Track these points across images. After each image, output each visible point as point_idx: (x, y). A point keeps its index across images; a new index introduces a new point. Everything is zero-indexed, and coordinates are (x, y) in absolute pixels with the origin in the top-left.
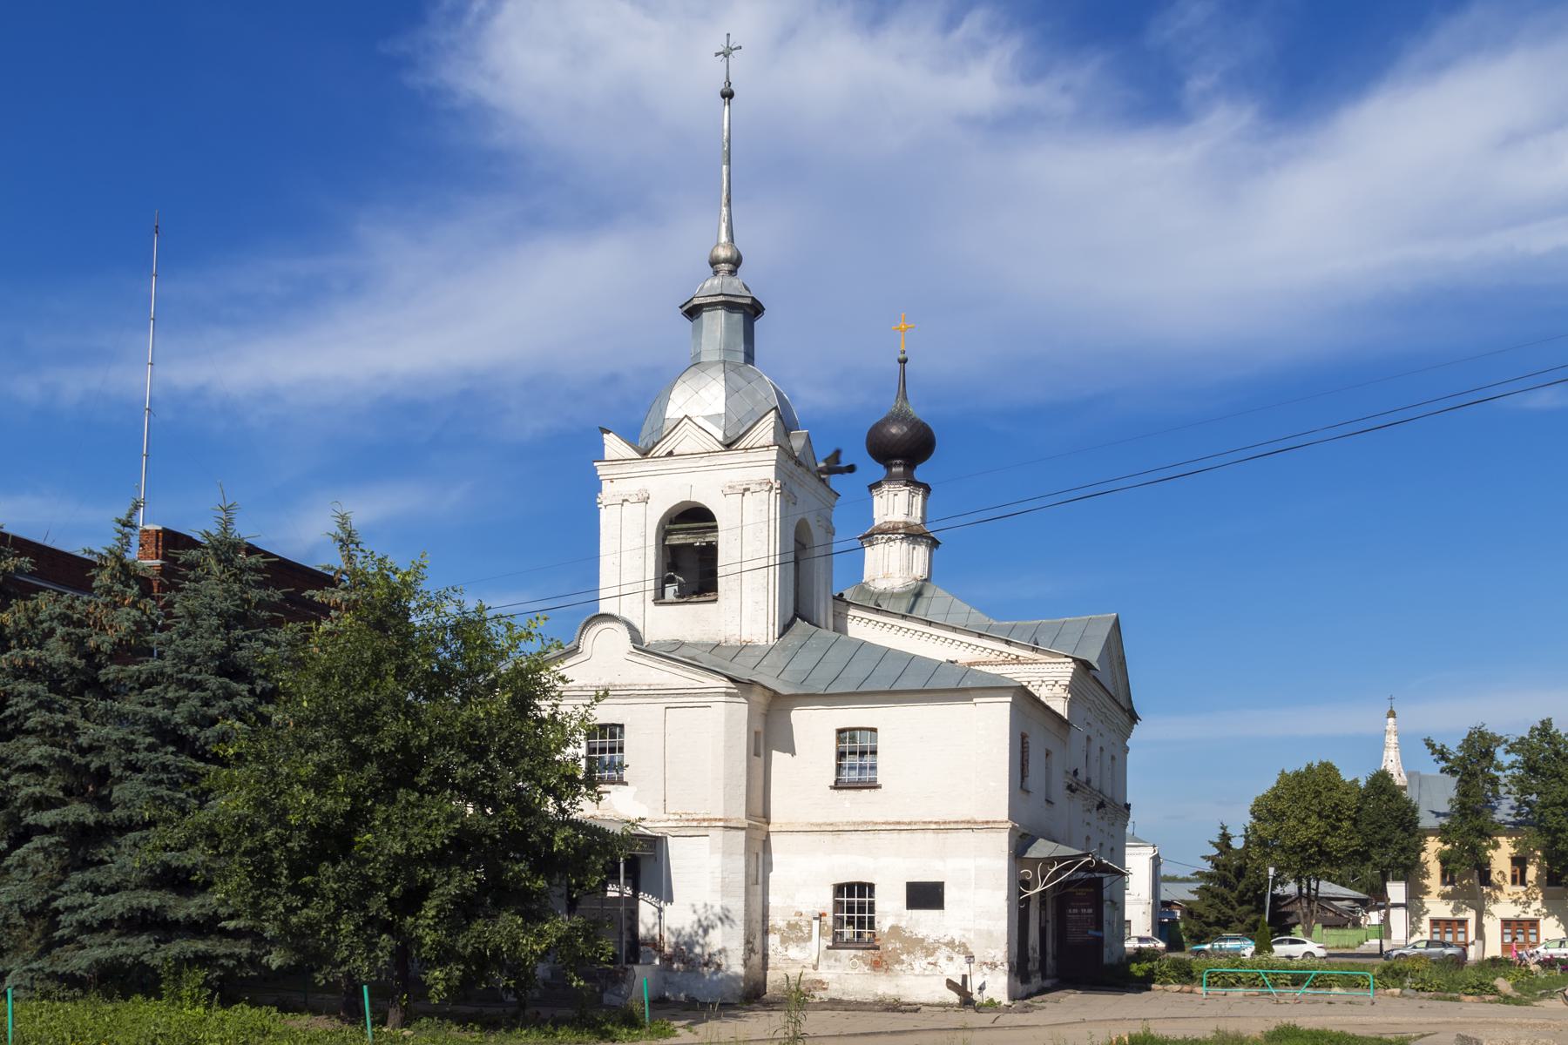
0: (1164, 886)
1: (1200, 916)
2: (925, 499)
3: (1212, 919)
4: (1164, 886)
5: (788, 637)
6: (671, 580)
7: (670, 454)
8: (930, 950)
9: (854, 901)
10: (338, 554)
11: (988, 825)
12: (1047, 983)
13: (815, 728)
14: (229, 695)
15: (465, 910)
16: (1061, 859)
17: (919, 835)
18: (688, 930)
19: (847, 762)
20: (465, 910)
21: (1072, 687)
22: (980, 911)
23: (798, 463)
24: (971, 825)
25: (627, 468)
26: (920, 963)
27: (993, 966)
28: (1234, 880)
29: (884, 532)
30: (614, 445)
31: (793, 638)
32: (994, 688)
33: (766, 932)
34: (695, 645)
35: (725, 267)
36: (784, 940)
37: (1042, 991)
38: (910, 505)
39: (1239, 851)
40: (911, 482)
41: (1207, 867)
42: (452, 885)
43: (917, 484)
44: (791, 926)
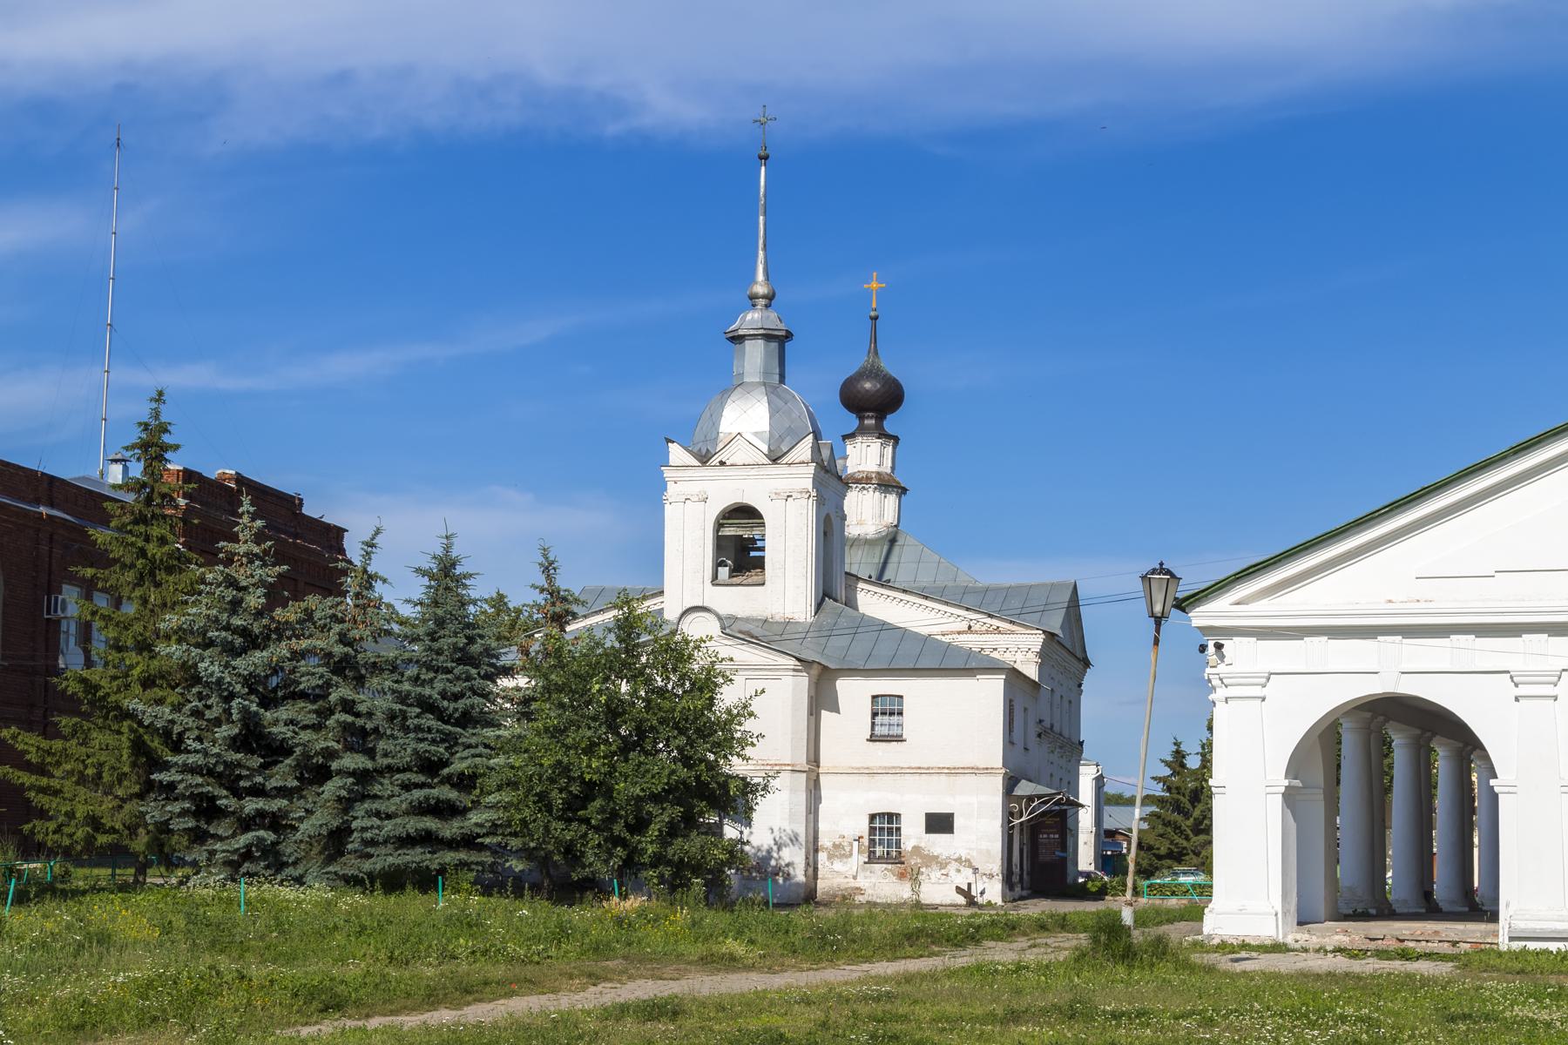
0: (1107, 809)
1: (1150, 848)
2: (894, 448)
3: (1163, 851)
4: (1107, 809)
5: (822, 615)
6: (722, 564)
7: (722, 463)
8: (943, 865)
9: (885, 825)
10: (543, 577)
11: (987, 771)
12: (1025, 893)
13: (855, 693)
14: (469, 678)
15: (672, 831)
16: (1039, 797)
17: (935, 777)
18: (765, 847)
19: (879, 719)
20: (672, 831)
21: (1042, 654)
22: (981, 837)
23: (827, 471)
24: (975, 771)
25: (764, 471)
26: (936, 874)
27: (991, 876)
28: (1188, 806)
29: (858, 481)
30: (677, 453)
31: (826, 618)
32: (992, 668)
33: (816, 851)
34: (747, 620)
35: (762, 302)
36: (830, 857)
37: (1022, 898)
38: (882, 456)
39: (1194, 772)
40: (883, 435)
41: (1158, 790)
42: (663, 816)
43: (888, 437)
44: (836, 846)
